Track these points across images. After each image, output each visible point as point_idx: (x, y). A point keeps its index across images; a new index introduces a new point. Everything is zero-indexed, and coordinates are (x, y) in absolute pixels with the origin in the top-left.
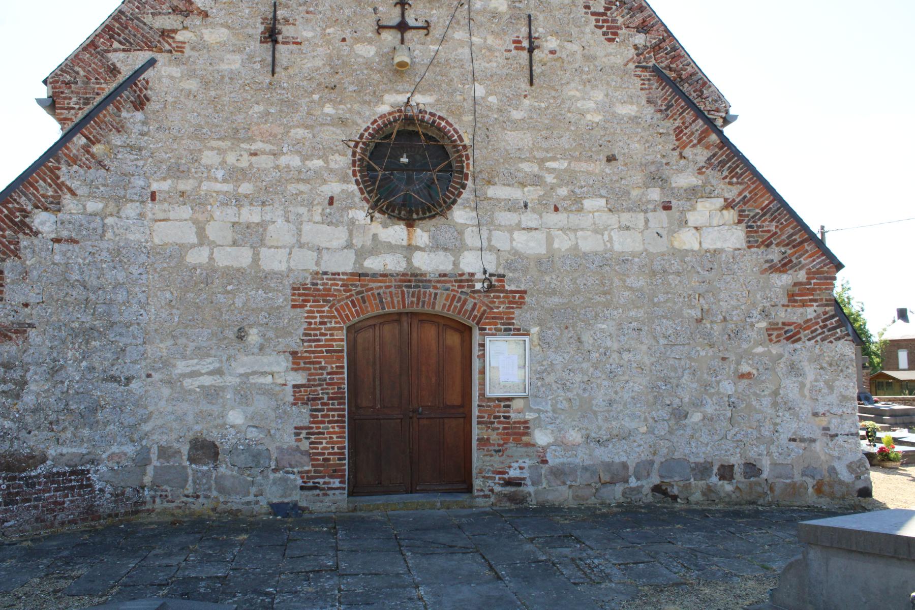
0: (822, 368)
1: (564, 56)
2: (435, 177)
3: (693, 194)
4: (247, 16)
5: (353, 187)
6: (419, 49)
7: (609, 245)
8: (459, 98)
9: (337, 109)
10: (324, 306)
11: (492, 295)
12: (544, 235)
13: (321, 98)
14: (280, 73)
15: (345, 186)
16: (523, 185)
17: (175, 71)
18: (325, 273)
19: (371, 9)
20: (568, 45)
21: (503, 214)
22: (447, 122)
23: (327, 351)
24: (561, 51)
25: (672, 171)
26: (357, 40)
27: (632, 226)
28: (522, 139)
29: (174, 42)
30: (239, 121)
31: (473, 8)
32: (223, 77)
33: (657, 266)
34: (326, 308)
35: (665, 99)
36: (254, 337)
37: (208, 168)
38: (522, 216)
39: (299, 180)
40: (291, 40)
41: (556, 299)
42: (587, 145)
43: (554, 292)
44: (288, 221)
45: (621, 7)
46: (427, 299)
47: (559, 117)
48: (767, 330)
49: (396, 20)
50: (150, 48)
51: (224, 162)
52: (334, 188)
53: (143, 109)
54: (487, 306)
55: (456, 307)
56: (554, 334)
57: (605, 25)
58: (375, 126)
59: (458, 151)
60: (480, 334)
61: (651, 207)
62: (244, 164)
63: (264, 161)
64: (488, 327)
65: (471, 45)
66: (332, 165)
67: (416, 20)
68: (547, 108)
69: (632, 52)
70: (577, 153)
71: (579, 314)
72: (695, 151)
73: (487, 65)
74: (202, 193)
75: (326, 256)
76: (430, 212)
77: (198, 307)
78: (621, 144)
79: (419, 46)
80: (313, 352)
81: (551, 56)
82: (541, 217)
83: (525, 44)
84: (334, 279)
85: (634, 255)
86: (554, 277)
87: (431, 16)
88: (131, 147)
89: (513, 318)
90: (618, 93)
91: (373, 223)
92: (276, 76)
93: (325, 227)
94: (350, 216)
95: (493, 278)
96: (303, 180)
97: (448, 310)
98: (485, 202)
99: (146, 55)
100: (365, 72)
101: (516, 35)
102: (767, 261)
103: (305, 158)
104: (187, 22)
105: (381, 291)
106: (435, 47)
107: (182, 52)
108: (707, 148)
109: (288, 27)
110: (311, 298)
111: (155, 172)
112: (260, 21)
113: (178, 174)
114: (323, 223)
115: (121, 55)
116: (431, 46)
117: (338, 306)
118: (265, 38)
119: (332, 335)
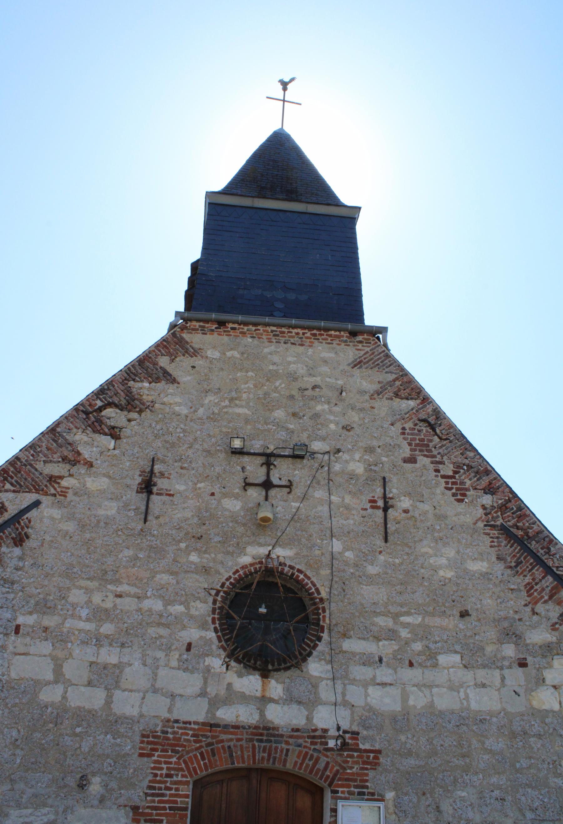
1: (417, 515)
2: (291, 628)
4: (127, 468)
5: (211, 635)
6: (281, 506)
7: (465, 703)
8: (317, 552)
9: (201, 558)
10: (170, 757)
11: (345, 753)
12: (399, 691)
13: (187, 547)
15: (203, 633)
16: (378, 639)
17: (56, 513)
18: (177, 721)
19: (239, 468)
20: (421, 505)
21: (358, 668)
22: (305, 575)
23: (170, 808)
24: (414, 511)
25: (525, 627)
26: (225, 495)
27: (488, 683)
28: (377, 594)
29: (59, 487)
30: (109, 563)
31: (332, 470)
32: (98, 522)
34: (174, 760)
35: (514, 556)
36: (96, 786)
37: (74, 606)
38: (377, 671)
39: (159, 624)
40: (164, 492)
41: (412, 761)
42: (440, 600)
43: (409, 753)
44: (145, 665)
45: (468, 470)
46: (278, 755)
47: (413, 573)
50: (37, 491)
51: (90, 601)
52: (193, 634)
53: (21, 545)
54: (340, 765)
55: (308, 765)
56: (410, 801)
57: (454, 486)
58: (236, 576)
59: (315, 604)
60: (332, 797)
61: (506, 663)
62: (108, 605)
63: (128, 604)
64: (340, 789)
65: (330, 503)
66: (193, 612)
67: (280, 479)
68: (402, 564)
69: (481, 511)
70: (431, 608)
71: (437, 778)
72: (547, 607)
73: (345, 522)
74: (65, 630)
75: (179, 703)
76: (285, 663)
77: (44, 749)
78: (473, 599)
79: (282, 503)
80: (156, 808)
81: (404, 515)
82: (396, 672)
83: (381, 503)
84: (185, 728)
85: (492, 714)
86: (410, 736)
87: (294, 476)
88: (5, 580)
89: (367, 781)
90: (468, 550)
91: (229, 672)
92: (147, 523)
94: (206, 664)
95: (347, 736)
96: (163, 624)
97: (300, 768)
98: (340, 656)
99: (31, 497)
100: (231, 524)
101: (371, 495)
103: (168, 603)
104: (74, 470)
105: (232, 744)
106: (297, 505)
107: (65, 496)
109: (162, 480)
110: (160, 747)
111: (23, 606)
112: (138, 473)
113: (45, 609)
114: (179, 669)
115: (11, 495)
116: (292, 504)
117: (186, 757)
118: (141, 488)
119: (177, 790)
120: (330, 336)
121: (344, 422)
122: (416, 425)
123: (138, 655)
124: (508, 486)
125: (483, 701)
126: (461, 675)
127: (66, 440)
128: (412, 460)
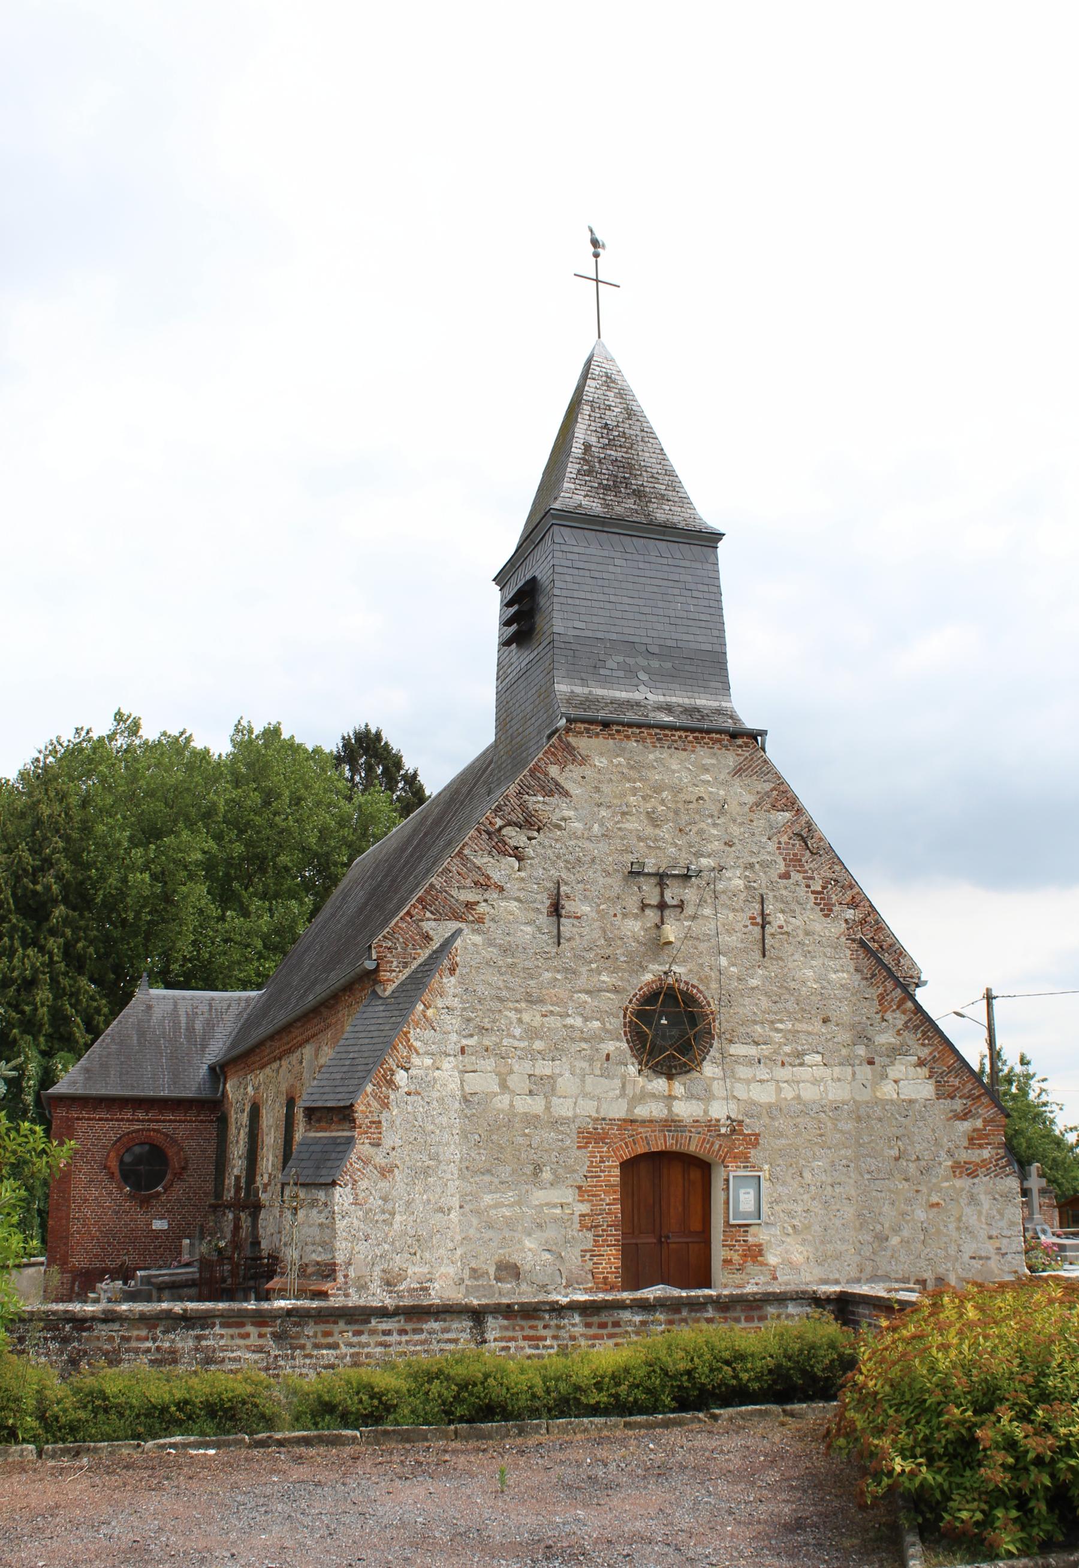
0: (995, 1199)
3: (895, 1052)
14: (565, 945)
15: (618, 1044)
17: (478, 939)
18: (604, 1119)
22: (698, 990)
33: (862, 1112)
34: (605, 1149)
36: (547, 1175)
48: (952, 1167)
52: (610, 1046)
80: (595, 1186)
83: (759, 920)
93: (602, 1080)
102: (951, 1111)
108: (904, 1013)
115: (433, 924)
120: (711, 739)
121: (727, 838)
122: (790, 838)
124: (868, 900)
126: (820, 1072)
127: (474, 864)
128: (786, 876)
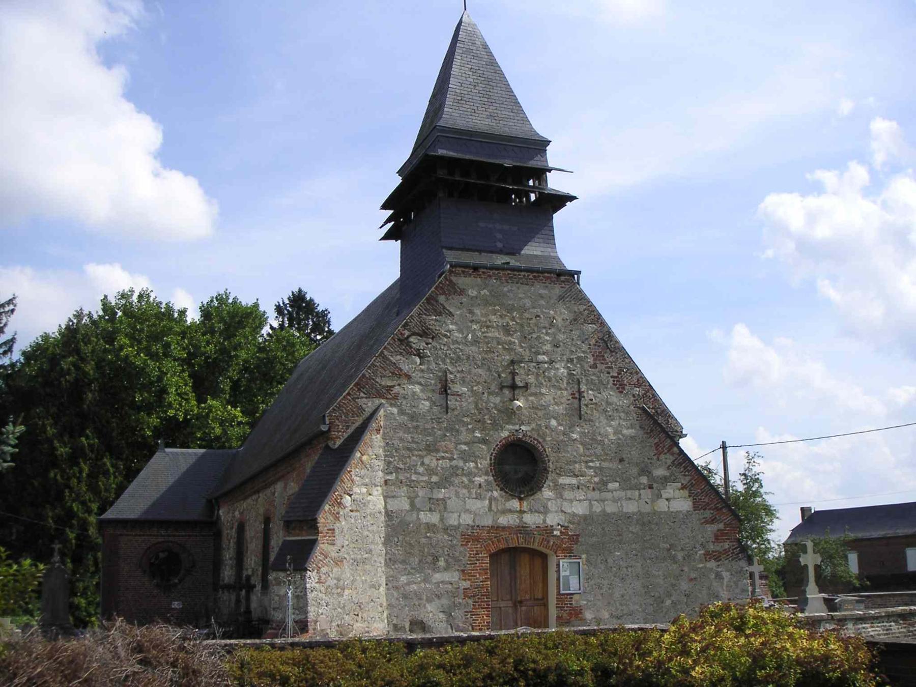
3: (665, 481)
33: (645, 520)
36: (442, 563)
41: (594, 539)
43: (593, 536)
49: (510, 382)
83: (577, 395)
123: (453, 492)
125: (631, 508)
